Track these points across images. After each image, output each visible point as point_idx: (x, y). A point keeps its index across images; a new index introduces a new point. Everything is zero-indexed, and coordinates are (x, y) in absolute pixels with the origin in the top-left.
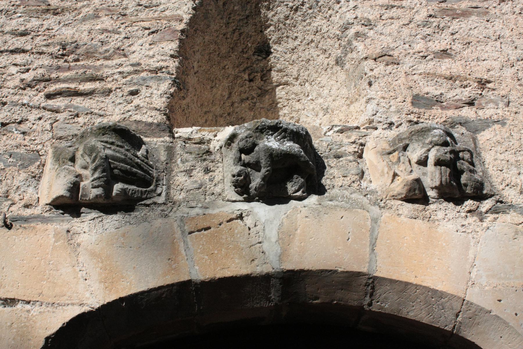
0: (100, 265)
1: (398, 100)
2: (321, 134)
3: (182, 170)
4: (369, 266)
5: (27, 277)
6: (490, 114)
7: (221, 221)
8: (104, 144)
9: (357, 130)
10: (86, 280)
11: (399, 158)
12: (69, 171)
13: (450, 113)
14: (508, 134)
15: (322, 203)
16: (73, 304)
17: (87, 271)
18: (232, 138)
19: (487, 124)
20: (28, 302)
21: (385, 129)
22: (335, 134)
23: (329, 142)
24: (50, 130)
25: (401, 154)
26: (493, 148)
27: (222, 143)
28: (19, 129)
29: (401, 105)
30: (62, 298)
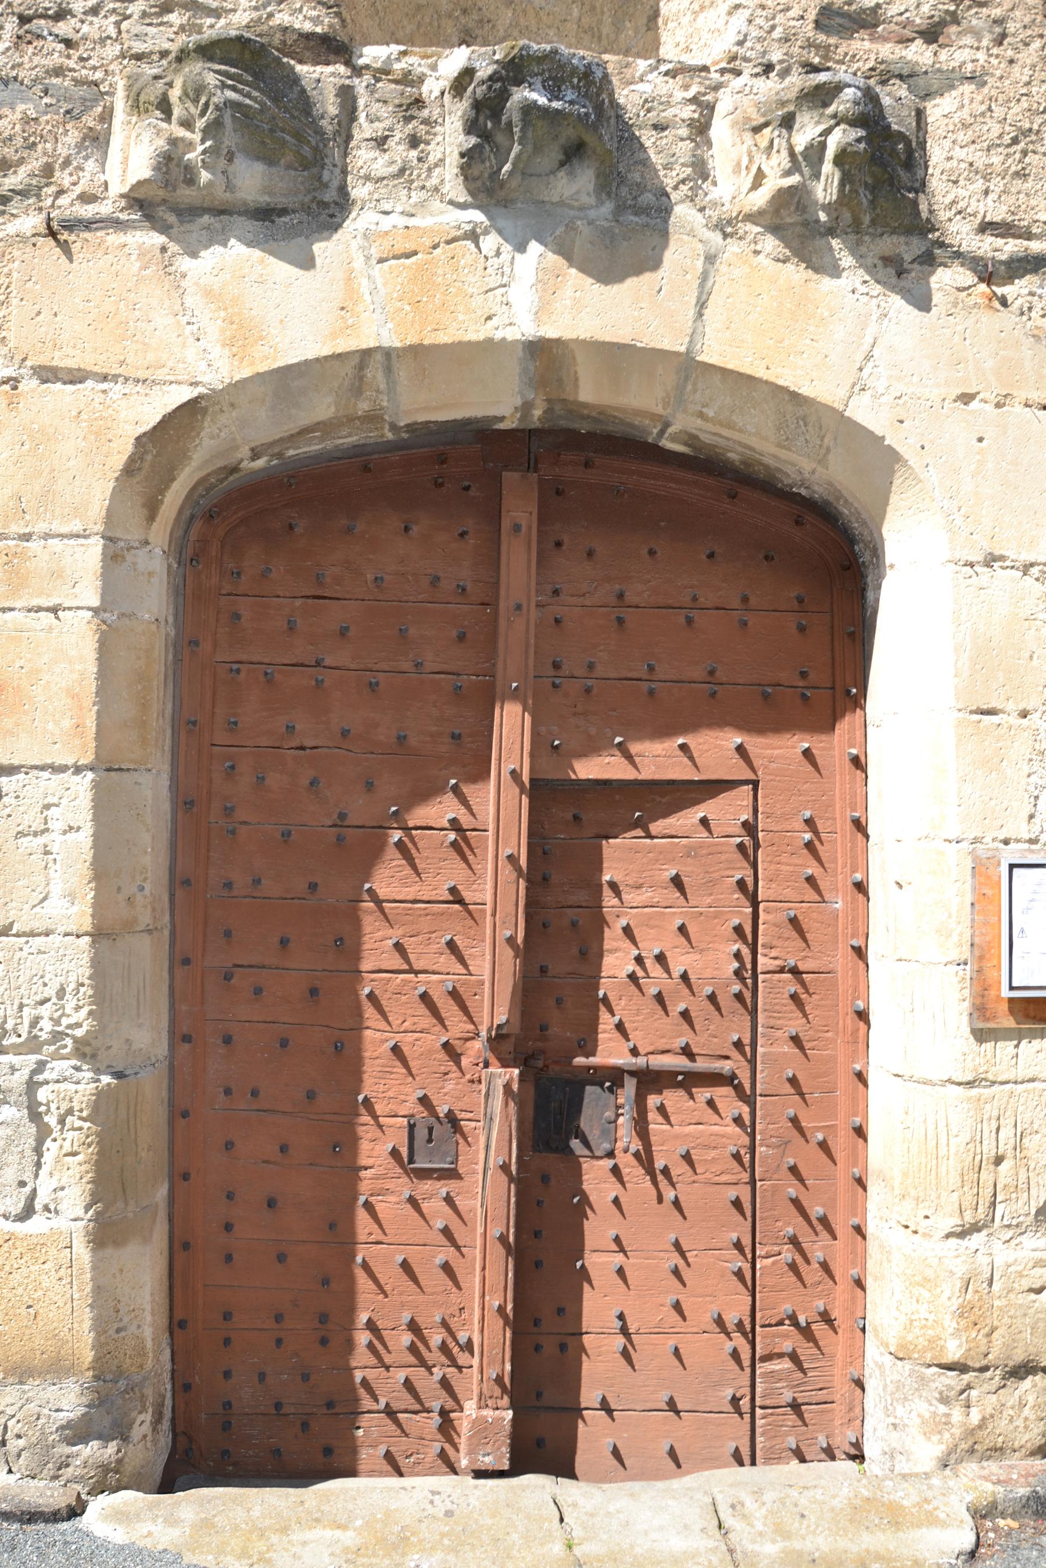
0: (222, 314)
1: (791, 14)
2: (633, 77)
3: (368, 136)
4: (691, 342)
5: (98, 332)
6: (961, 59)
7: (437, 241)
8: (220, 78)
9: (703, 74)
10: (198, 340)
11: (772, 142)
12: (159, 130)
13: (887, 50)
14: (984, 108)
15: (621, 219)
16: (179, 383)
17: (201, 324)
18: (468, 73)
19: (950, 80)
20: (105, 378)
21: (756, 75)
22: (661, 78)
23: (647, 95)
24: (114, 36)
25: (776, 133)
26: (950, 134)
27: (444, 84)
28: (56, 31)
29: (794, 27)
30: (160, 371)
